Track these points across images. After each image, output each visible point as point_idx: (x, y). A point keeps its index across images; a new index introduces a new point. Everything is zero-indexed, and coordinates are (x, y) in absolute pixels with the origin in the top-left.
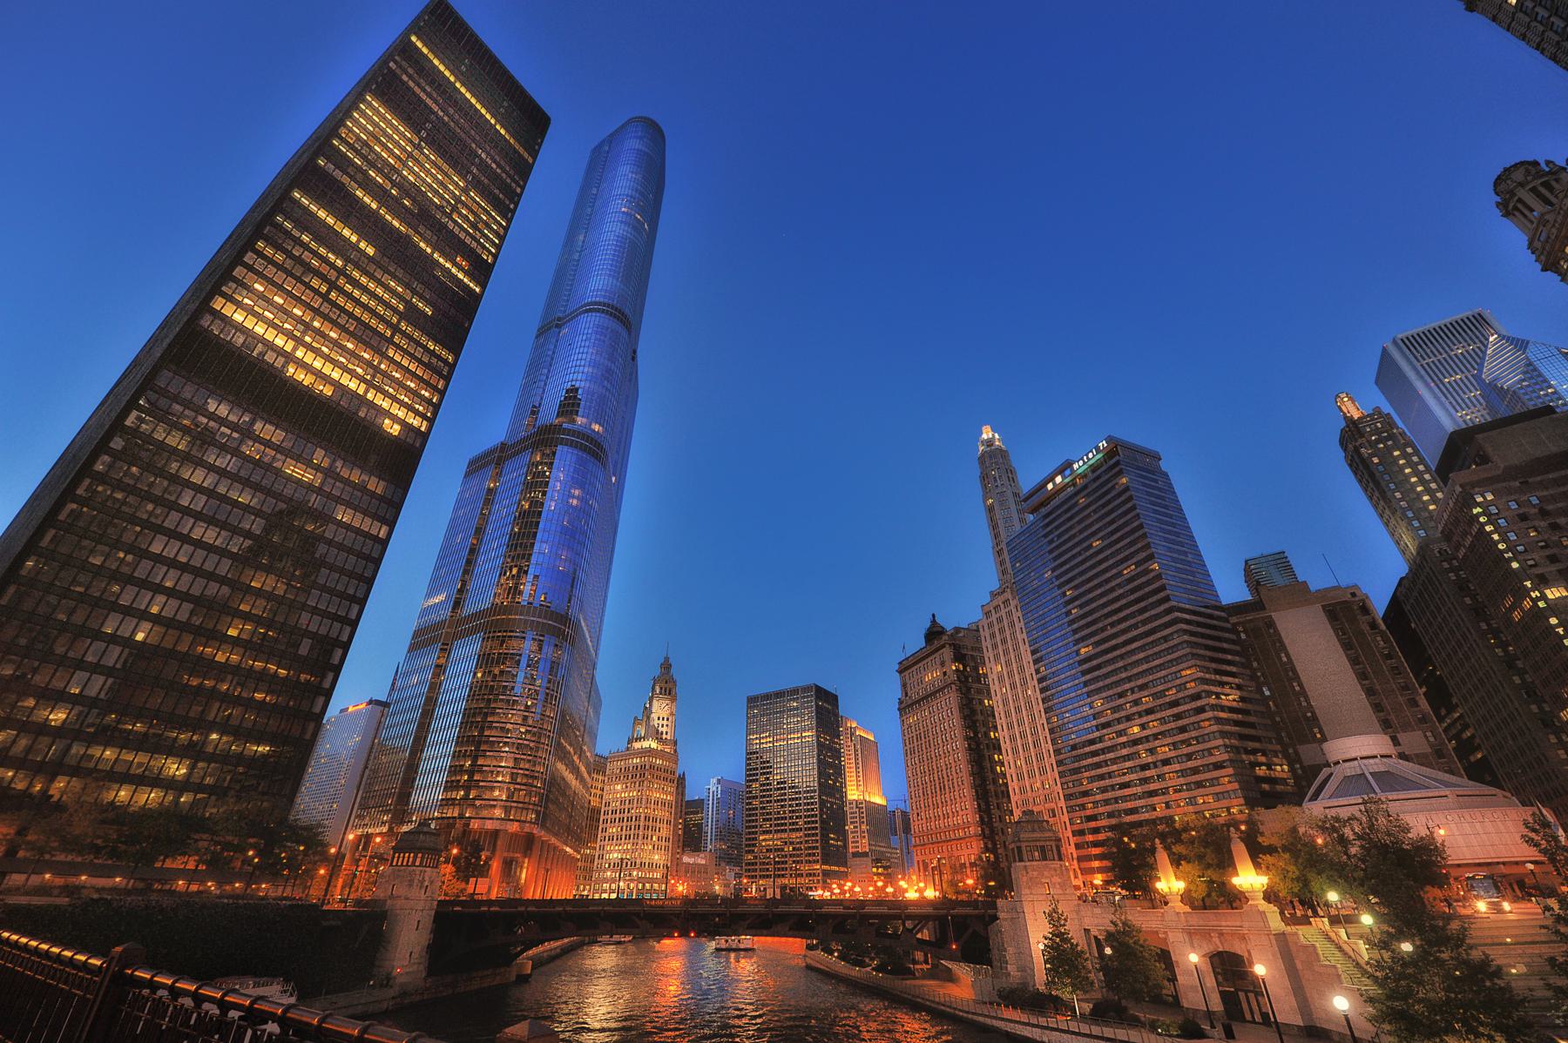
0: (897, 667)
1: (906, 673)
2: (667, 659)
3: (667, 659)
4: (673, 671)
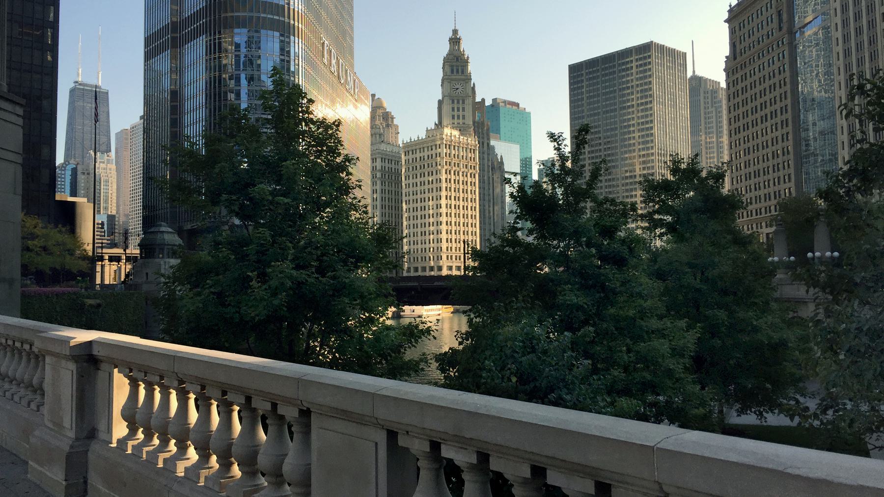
2: (455, 32)
3: (455, 32)
4: (463, 46)
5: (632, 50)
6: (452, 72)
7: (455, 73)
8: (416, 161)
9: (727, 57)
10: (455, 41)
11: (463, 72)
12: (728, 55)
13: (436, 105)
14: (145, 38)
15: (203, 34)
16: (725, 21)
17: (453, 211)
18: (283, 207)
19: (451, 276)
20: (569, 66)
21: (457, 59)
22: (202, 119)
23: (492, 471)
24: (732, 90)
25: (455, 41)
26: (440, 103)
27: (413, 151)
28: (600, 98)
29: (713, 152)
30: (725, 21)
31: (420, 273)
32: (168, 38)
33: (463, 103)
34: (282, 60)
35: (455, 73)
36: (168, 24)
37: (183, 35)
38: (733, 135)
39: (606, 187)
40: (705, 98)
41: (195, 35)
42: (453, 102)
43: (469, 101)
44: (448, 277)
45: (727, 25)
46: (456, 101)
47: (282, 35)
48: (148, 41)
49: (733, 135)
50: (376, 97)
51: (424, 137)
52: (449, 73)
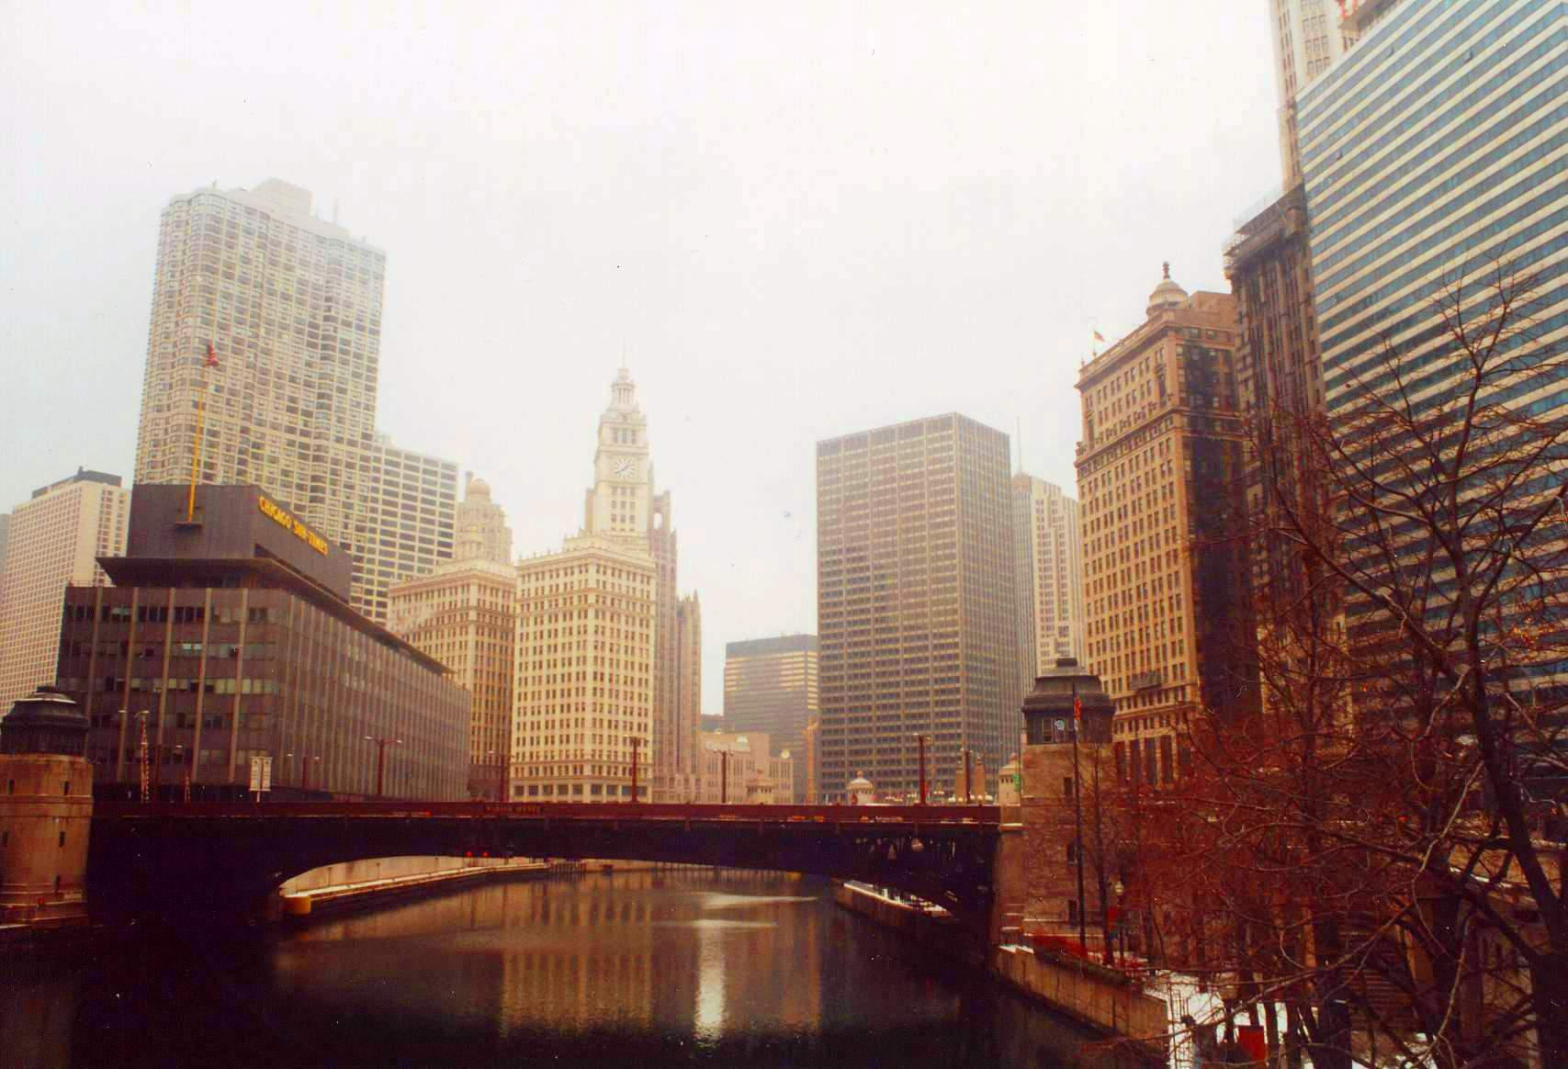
0: (1077, 378)
1: (1093, 391)
3: (623, 372)
5: (866, 437)
6: (615, 440)
7: (620, 443)
9: (1079, 444)
10: (623, 387)
11: (634, 441)
12: (1080, 439)
13: (584, 497)
19: (616, 804)
20: (826, 449)
21: (625, 417)
23: (1452, 848)
24: (1088, 498)
25: (623, 387)
26: (591, 494)
28: (897, 538)
29: (1051, 577)
31: (541, 798)
33: (633, 494)
35: (620, 443)
39: (906, 672)
40: (1038, 511)
42: (614, 493)
43: (642, 492)
44: (595, 807)
45: (1078, 392)
50: (474, 478)
51: (560, 551)
52: (609, 441)
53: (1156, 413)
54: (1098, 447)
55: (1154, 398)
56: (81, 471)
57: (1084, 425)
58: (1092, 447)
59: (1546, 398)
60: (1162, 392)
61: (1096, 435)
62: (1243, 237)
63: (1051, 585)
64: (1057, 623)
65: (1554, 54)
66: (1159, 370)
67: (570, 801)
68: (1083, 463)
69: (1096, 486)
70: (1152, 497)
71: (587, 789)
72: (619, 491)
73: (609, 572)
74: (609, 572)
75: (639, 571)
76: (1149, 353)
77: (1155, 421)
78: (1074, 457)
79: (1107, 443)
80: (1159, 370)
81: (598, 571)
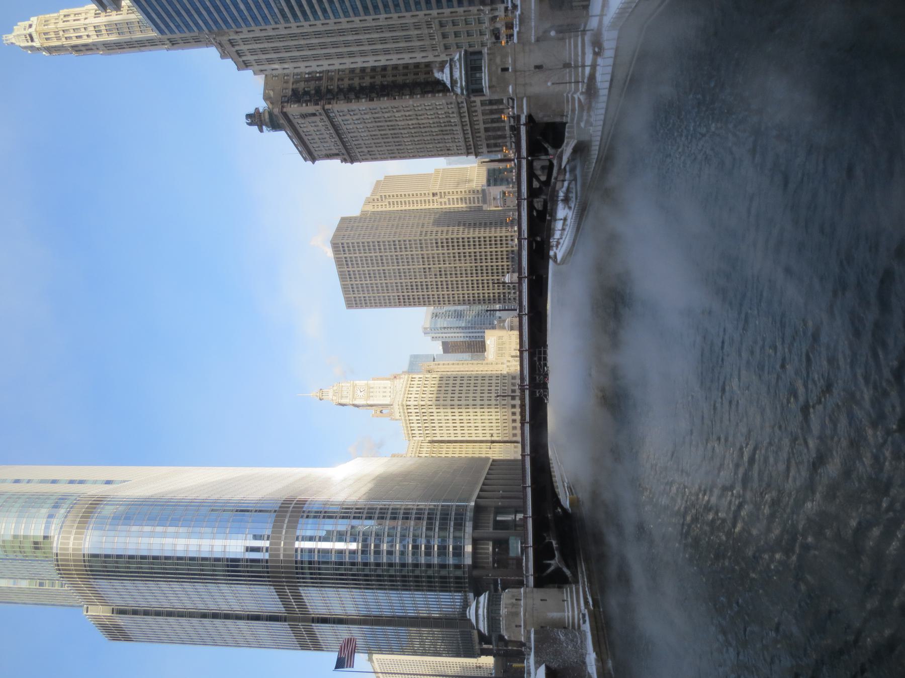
0: (309, 163)
1: (315, 154)
8: (433, 430)
9: (342, 162)
12: (340, 161)
14: (302, 649)
15: (298, 589)
16: (313, 163)
17: (443, 418)
18: (716, 517)
20: (351, 303)
22: (395, 630)
27: (412, 430)
30: (313, 163)
32: (302, 625)
34: (268, 539)
36: (289, 625)
37: (299, 611)
38: (375, 157)
41: (298, 597)
45: (317, 162)
46: (371, 394)
47: (302, 517)
48: (304, 647)
49: (375, 157)
53: (325, 119)
54: (344, 151)
55: (317, 119)
56: (369, 661)
57: (334, 159)
58: (343, 154)
59: (234, 22)
60: (314, 115)
61: (337, 152)
62: (264, 128)
63: (458, 203)
64: (431, 198)
65: (178, 6)
66: (304, 116)
67: (520, 410)
68: (351, 159)
69: (362, 152)
70: (394, 136)
71: (513, 402)
72: (371, 394)
73: (410, 396)
74: (410, 396)
75: (406, 395)
76: (295, 121)
77: (329, 120)
78: (349, 164)
79: (341, 147)
80: (304, 116)
81: (410, 401)
